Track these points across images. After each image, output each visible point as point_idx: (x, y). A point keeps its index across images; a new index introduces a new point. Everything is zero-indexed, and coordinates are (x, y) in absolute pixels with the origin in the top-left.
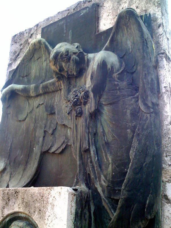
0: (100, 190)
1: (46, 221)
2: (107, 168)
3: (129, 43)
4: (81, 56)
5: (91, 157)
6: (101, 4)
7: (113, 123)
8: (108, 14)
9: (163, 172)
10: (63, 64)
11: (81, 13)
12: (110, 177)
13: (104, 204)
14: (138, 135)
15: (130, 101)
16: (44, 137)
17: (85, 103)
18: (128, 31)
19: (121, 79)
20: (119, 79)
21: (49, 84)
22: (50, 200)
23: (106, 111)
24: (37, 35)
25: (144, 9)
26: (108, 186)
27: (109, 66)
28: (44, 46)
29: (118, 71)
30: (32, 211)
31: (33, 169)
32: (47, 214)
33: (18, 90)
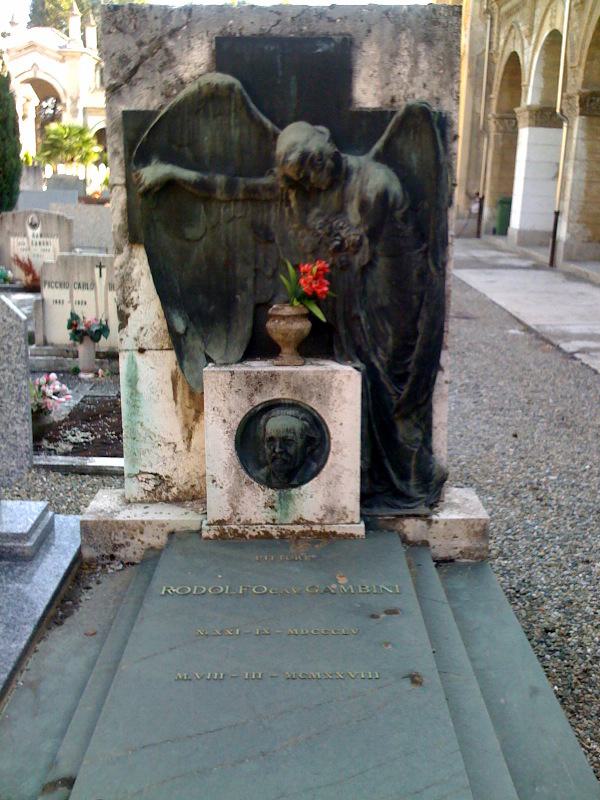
0: (377, 364)
1: (331, 407)
2: (386, 340)
3: (414, 157)
4: (337, 158)
5: (361, 326)
6: (357, 43)
7: (291, 153)
8: (371, 72)
9: (445, 334)
10: (312, 174)
11: (317, 48)
12: (390, 351)
13: (382, 379)
14: (427, 304)
15: (416, 255)
16: (255, 278)
17: (356, 252)
18: (414, 139)
19: (405, 219)
20: (402, 219)
21: (260, 188)
22: (335, 384)
23: (382, 263)
24: (192, 40)
25: (435, 94)
26: (388, 362)
27: (391, 199)
28: (239, 97)
29: (401, 207)
30: (307, 397)
31: (246, 330)
32: (332, 399)
33: (185, 182)
